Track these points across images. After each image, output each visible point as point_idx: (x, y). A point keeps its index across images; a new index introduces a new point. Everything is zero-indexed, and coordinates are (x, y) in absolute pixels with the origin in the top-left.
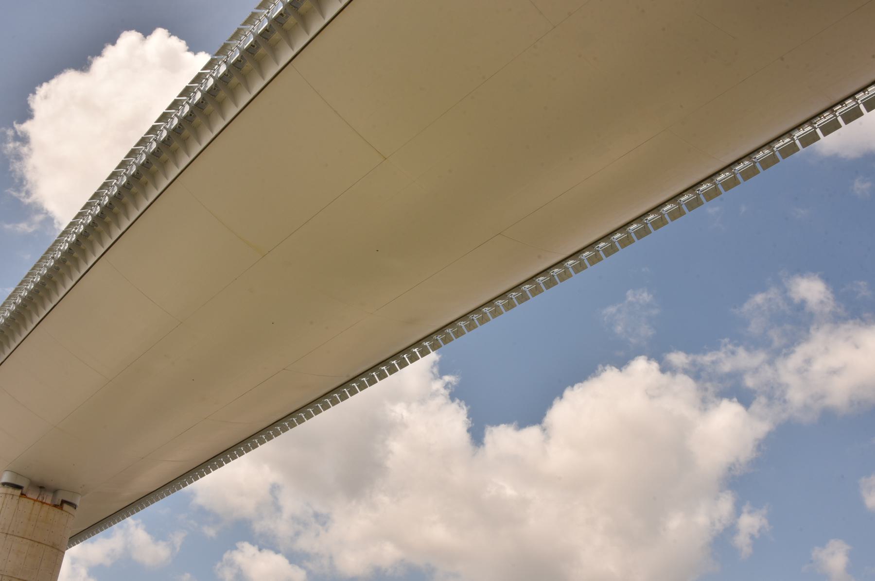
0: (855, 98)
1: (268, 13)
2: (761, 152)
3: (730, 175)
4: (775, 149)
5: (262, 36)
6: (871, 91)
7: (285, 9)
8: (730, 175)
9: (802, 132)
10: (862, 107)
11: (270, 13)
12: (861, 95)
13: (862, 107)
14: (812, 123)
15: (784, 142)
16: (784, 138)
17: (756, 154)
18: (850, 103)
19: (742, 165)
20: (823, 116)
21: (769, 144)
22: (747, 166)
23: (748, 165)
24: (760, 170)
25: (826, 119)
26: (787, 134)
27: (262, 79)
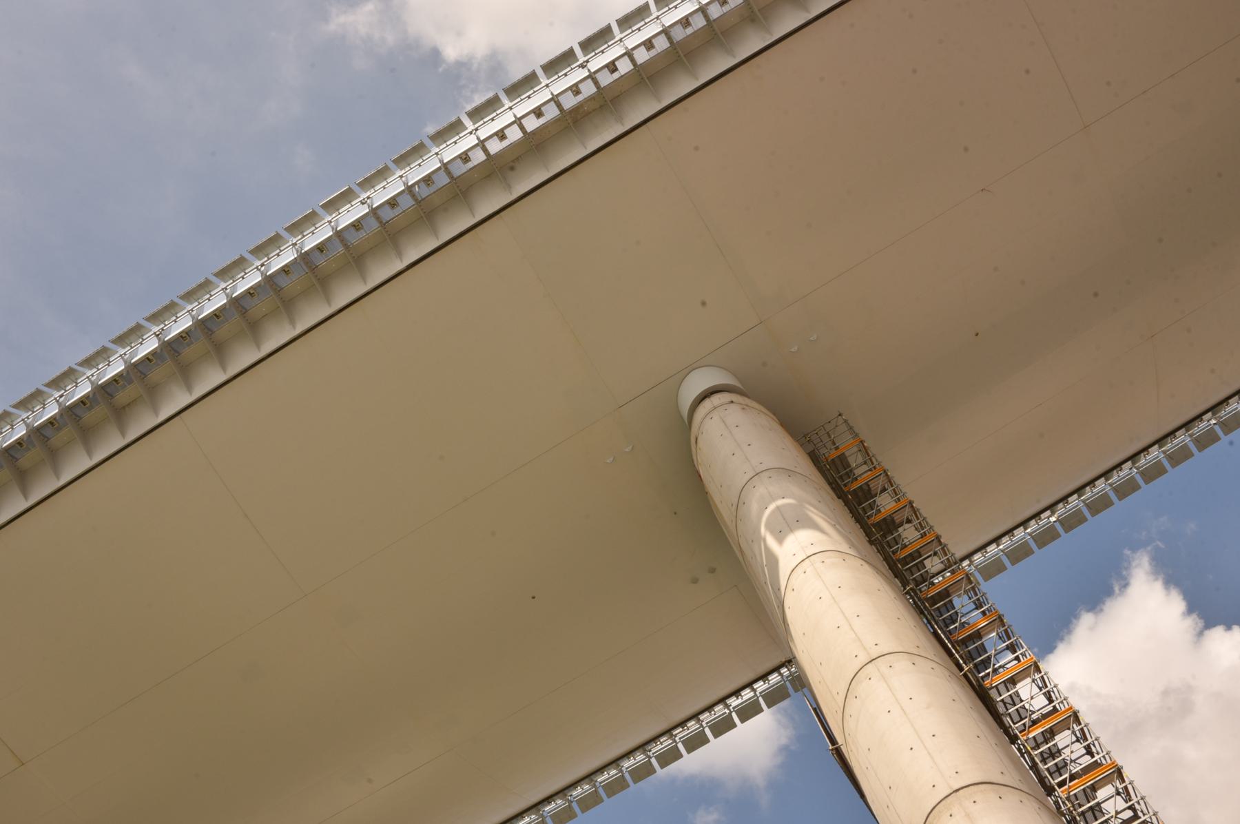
0: (699, 720)
1: (61, 396)
2: (579, 788)
3: (537, 819)
4: (597, 784)
5: (39, 432)
6: (718, 711)
7: (29, 436)
8: (537, 819)
9: (632, 761)
10: (708, 731)
11: (63, 397)
12: (706, 716)
13: (708, 731)
14: (645, 750)
15: (635, 759)
16: (609, 769)
17: (572, 790)
18: (719, 709)
19: (553, 804)
20: (659, 741)
21: (589, 777)
22: (560, 806)
23: (587, 791)
24: (1087, 516)
25: (663, 746)
26: (614, 765)
27: (222, 372)
